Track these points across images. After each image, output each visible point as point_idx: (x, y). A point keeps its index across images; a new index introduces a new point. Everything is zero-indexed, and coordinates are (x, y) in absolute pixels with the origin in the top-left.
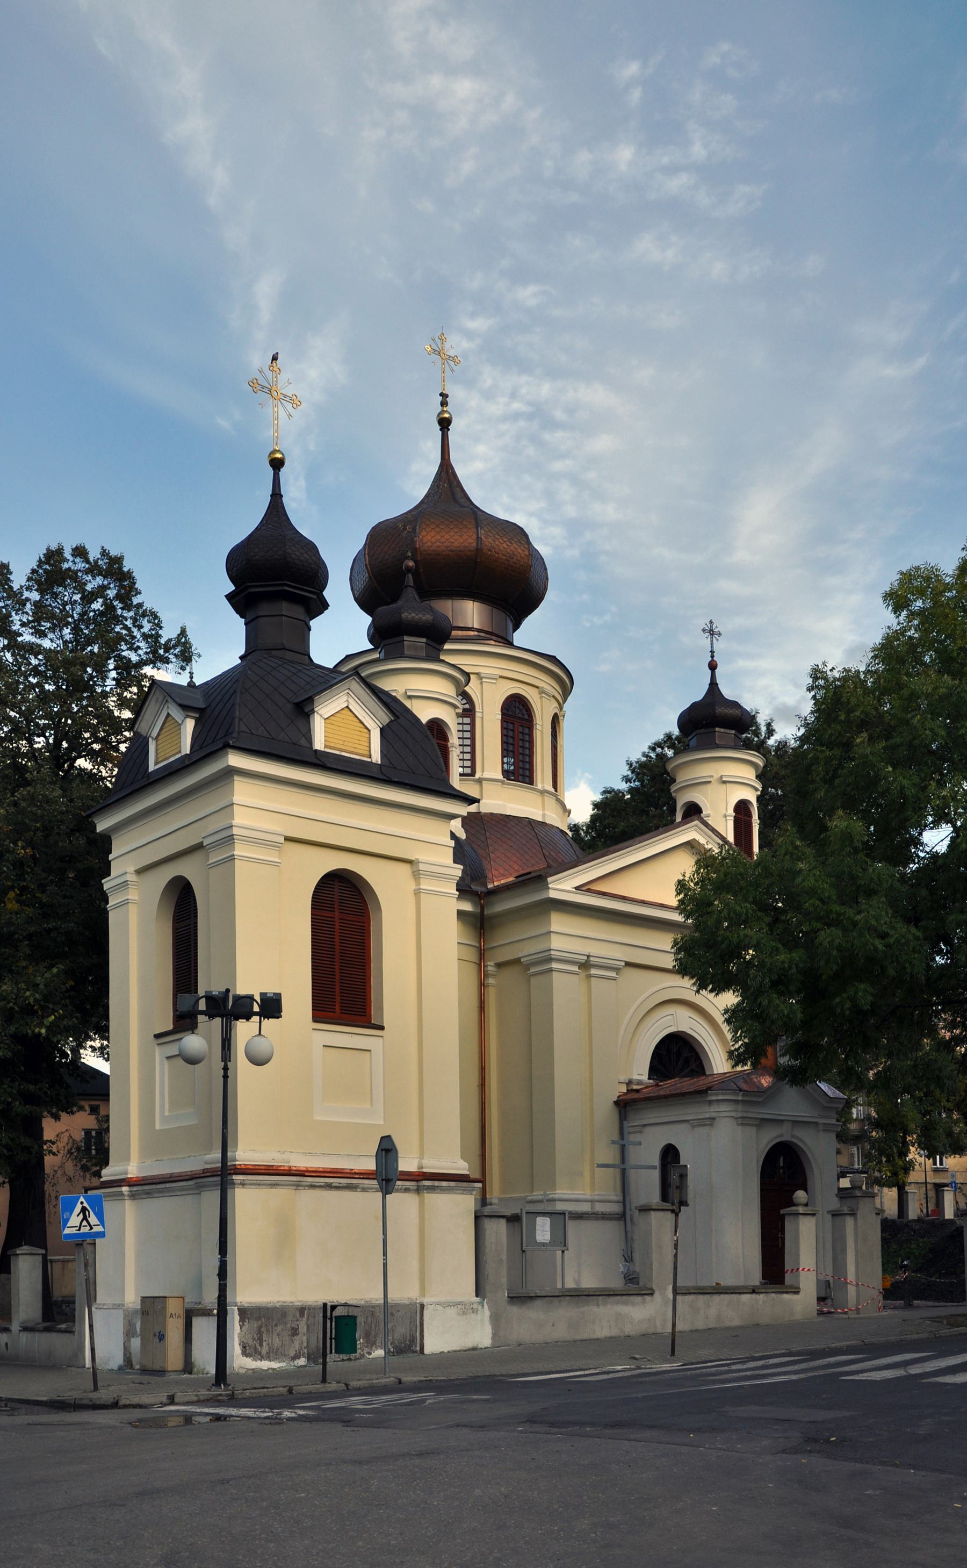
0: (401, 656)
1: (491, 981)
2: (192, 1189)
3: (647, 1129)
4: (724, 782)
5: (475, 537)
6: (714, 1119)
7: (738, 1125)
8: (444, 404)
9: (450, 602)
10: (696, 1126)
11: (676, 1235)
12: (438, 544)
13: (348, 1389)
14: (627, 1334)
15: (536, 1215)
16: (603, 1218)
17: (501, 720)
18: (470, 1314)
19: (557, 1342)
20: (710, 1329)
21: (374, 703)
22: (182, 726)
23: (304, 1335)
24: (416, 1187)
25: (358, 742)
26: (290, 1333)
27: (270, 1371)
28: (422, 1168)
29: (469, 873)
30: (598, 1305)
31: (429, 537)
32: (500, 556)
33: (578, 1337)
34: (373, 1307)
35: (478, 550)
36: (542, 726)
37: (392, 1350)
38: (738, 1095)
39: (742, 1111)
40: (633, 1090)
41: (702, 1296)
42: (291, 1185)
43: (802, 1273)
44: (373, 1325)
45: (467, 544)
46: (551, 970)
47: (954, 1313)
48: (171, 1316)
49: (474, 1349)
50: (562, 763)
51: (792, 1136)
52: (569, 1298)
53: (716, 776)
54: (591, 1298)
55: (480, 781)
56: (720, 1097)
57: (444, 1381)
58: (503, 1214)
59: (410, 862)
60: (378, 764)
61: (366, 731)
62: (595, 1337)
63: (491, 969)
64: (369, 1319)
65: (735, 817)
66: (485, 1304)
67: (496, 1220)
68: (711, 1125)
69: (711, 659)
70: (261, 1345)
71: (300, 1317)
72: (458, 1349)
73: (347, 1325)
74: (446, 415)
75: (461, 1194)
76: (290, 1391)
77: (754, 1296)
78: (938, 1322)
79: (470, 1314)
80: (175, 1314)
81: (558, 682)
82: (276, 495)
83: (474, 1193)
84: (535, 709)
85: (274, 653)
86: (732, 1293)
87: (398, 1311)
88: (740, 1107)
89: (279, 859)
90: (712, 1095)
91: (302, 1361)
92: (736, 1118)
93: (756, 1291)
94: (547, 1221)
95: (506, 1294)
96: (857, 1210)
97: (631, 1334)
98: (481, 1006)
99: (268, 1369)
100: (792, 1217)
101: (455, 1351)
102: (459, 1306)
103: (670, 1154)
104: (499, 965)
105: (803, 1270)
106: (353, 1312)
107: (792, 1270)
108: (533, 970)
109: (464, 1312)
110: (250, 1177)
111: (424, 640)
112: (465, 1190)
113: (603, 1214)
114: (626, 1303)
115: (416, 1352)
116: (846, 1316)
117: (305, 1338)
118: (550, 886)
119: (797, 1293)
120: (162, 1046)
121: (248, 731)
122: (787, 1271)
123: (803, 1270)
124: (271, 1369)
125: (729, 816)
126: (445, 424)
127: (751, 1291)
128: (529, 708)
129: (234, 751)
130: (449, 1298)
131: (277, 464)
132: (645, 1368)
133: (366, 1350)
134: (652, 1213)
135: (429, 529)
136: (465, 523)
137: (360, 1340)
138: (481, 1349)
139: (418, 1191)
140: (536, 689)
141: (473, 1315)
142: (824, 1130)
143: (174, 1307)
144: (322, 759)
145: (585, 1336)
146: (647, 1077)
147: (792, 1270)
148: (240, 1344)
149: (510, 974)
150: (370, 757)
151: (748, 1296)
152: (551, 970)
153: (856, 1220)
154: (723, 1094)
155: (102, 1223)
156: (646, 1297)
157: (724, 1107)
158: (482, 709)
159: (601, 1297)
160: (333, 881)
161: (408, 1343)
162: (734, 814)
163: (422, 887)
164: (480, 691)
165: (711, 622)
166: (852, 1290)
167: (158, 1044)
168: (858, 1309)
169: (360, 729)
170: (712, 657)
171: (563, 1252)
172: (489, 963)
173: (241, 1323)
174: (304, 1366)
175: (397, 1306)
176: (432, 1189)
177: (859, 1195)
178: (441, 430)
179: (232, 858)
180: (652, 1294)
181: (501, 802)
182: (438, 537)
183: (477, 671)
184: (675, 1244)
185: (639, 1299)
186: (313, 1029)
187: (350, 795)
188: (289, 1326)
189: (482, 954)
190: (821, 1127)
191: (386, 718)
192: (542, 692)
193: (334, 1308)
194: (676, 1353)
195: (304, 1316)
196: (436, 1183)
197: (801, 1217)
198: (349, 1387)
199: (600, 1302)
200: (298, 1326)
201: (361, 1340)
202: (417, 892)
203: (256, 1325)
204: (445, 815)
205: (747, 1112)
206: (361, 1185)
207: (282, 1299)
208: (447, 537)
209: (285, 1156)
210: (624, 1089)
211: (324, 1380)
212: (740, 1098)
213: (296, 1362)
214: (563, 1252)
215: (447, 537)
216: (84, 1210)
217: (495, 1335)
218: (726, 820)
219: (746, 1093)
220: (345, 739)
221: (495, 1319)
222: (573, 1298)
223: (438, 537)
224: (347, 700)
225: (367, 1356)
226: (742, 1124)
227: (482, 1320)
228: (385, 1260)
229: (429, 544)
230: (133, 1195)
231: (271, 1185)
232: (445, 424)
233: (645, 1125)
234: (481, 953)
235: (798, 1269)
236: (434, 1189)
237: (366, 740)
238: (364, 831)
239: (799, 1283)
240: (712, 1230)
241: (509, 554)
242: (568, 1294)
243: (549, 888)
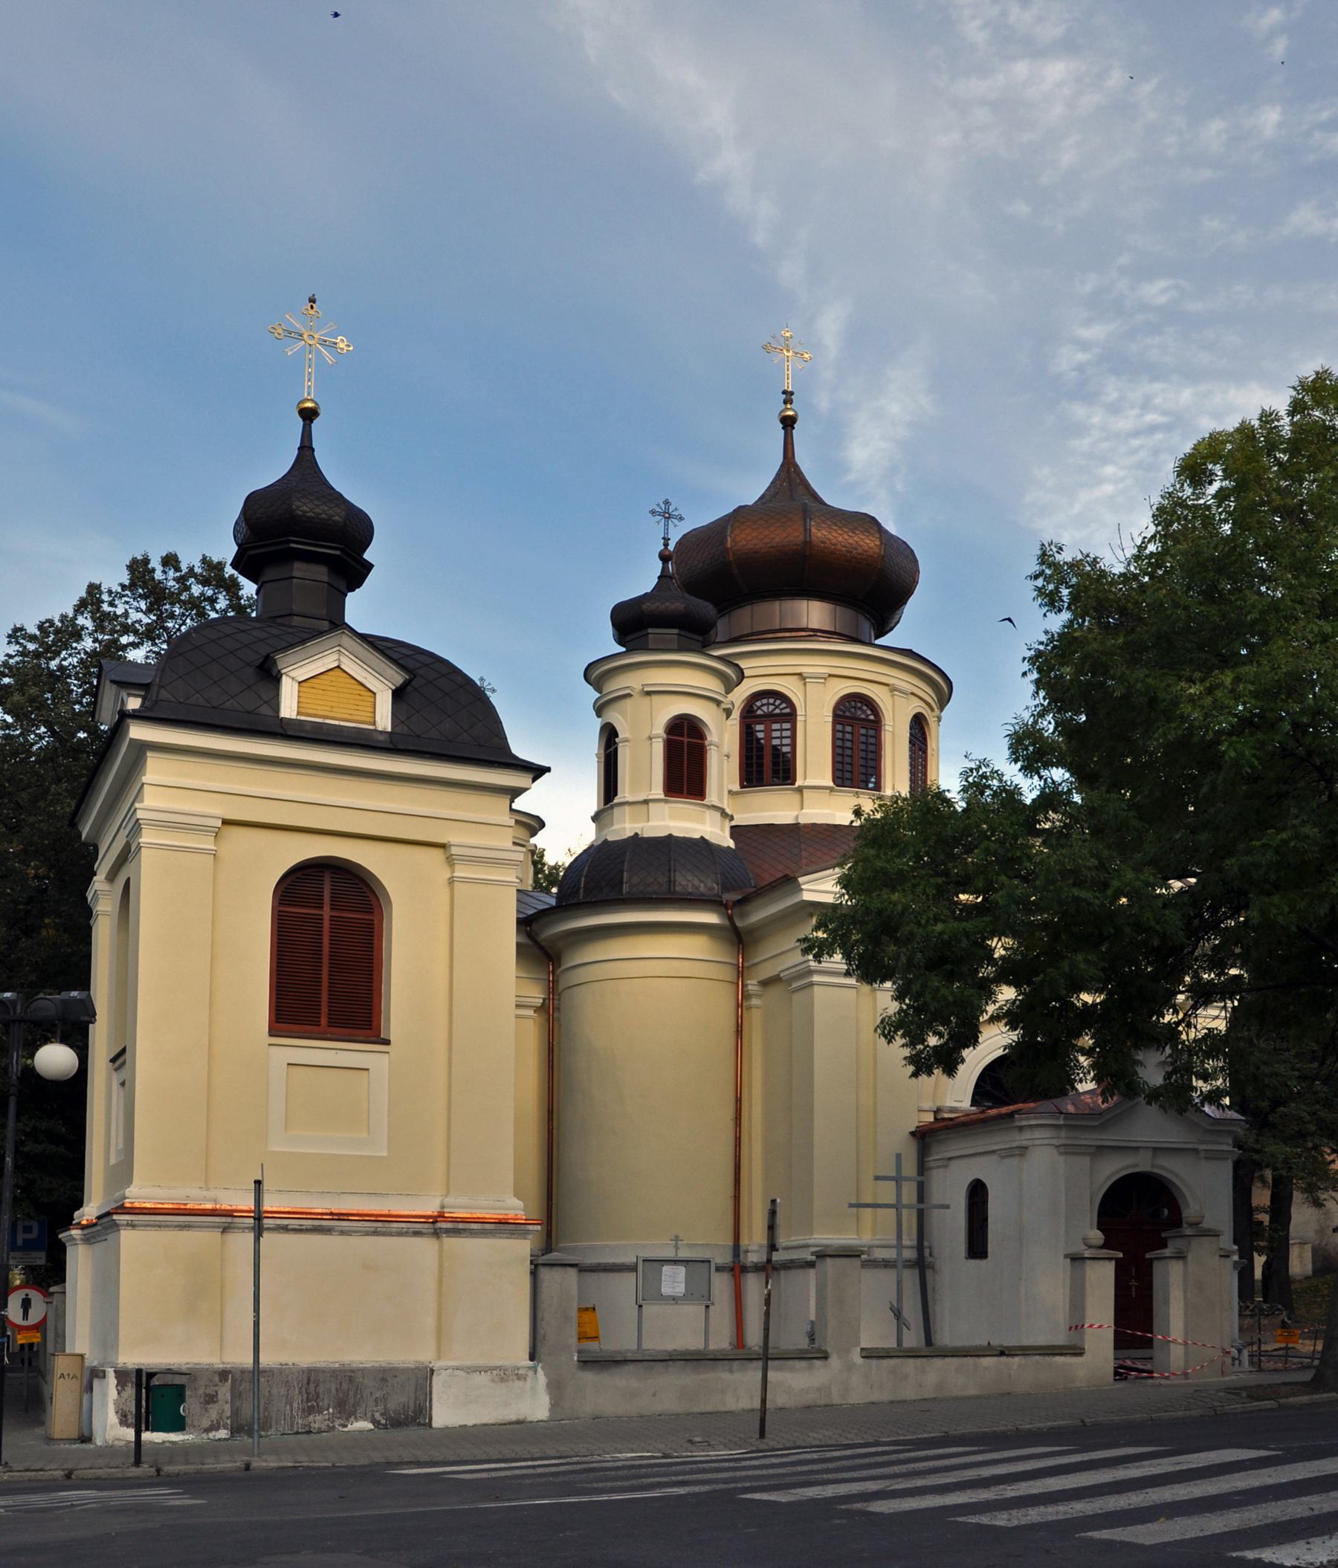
0: (645, 648)
1: (754, 1002)
3: (954, 1164)
4: (649, 693)
5: (801, 529)
6: (1026, 1148)
7: (1061, 1154)
9: (777, 603)
11: (767, 1287)
12: (755, 541)
13: (158, 1475)
14: (780, 1405)
15: (663, 1263)
16: (886, 1266)
17: (796, 715)
18: (513, 1381)
19: (659, 1415)
20: (925, 1400)
21: (378, 661)
23: (227, 1402)
24: (432, 1231)
25: (356, 707)
26: (202, 1400)
27: (167, 1444)
29: (720, 882)
30: (731, 1371)
31: (744, 536)
32: (839, 547)
34: (353, 1371)
35: (807, 543)
36: (893, 727)
37: (383, 1422)
38: (1058, 1118)
39: (1067, 1138)
40: (944, 1119)
41: (911, 1361)
42: (214, 1227)
43: (1088, 1331)
44: (351, 1393)
45: (792, 539)
46: (812, 984)
47: (703, 1411)
48: (62, 1376)
49: (519, 1422)
50: (934, 768)
52: (683, 1362)
53: (638, 687)
55: (800, 790)
57: (326, 1468)
58: (573, 1262)
59: (443, 846)
60: (388, 732)
61: (370, 694)
62: (726, 1409)
63: (752, 985)
64: (345, 1386)
66: (539, 1369)
67: (560, 1270)
68: (1022, 1155)
69: (663, 547)
71: (221, 1381)
72: (492, 1422)
73: (163, 1396)
74: (790, 413)
75: (508, 1238)
76: (247, 1467)
77: (1003, 1359)
78: (1234, 1394)
79: (513, 1381)
80: (69, 1375)
81: (922, 679)
82: (306, 448)
83: (530, 1237)
84: (883, 710)
85: (279, 620)
86: (966, 1356)
87: (396, 1376)
88: (1063, 1134)
89: (215, 846)
90: (1021, 1120)
91: (223, 1434)
93: (1007, 1352)
94: (681, 1270)
95: (576, 1358)
96: (1188, 1252)
97: (788, 1405)
98: (738, 1030)
99: (164, 1442)
101: (485, 1425)
102: (495, 1372)
103: (977, 1193)
104: (765, 983)
106: (178, 1380)
107: (1077, 1327)
108: (795, 985)
109: (502, 1378)
110: (141, 1217)
111: (676, 631)
112: (512, 1234)
113: (883, 1260)
116: (1168, 1382)
117: (227, 1407)
118: (803, 887)
119: (1081, 1354)
121: (174, 700)
123: (1091, 1326)
124: (169, 1442)
126: (788, 423)
127: (998, 1353)
128: (874, 707)
129: (135, 721)
130: (482, 1362)
131: (309, 415)
132: (677, 1457)
134: (829, 1260)
137: (328, 1410)
138: (531, 1422)
140: (886, 687)
141: (518, 1384)
142: (1207, 1158)
146: (970, 1103)
147: (1077, 1327)
148: (117, 1413)
149: (775, 992)
150: (374, 724)
151: (995, 1359)
152: (812, 984)
153: (1186, 1264)
154: (1036, 1118)
156: (815, 1361)
157: (1037, 1134)
158: (806, 712)
160: (323, 872)
161: (410, 1413)
162: (665, 736)
164: (803, 693)
168: (1185, 1375)
169: (359, 692)
171: (707, 1307)
172: (749, 982)
173: (119, 1388)
174: (225, 1439)
175: (269, 1372)
178: (783, 428)
180: (826, 1358)
181: (828, 811)
182: (755, 534)
183: (799, 671)
184: (766, 1300)
185: (803, 1363)
186: (269, 1045)
187: (327, 768)
189: (741, 972)
191: (399, 678)
192: (893, 689)
193: (151, 1375)
195: (227, 1380)
197: (1088, 1262)
198: (162, 1473)
200: (216, 1392)
201: (331, 1410)
202: (451, 881)
204: (500, 789)
206: (336, 1228)
208: (766, 532)
210: (930, 1118)
211: (138, 1462)
212: (1062, 1122)
213: (211, 1435)
214: (707, 1307)
215: (766, 532)
217: (554, 1406)
221: (556, 1388)
222: (688, 1363)
223: (755, 534)
224: (339, 659)
225: (340, 1428)
226: (1066, 1153)
227: (533, 1389)
229: (744, 543)
230: (88, 1240)
231: (179, 1226)
232: (788, 423)
233: (950, 1159)
234: (738, 971)
235: (1083, 1326)
236: (460, 1233)
238: (351, 810)
239: (1084, 1342)
240: (1020, 1279)
241: (851, 544)
242: (679, 1357)
243: (802, 890)
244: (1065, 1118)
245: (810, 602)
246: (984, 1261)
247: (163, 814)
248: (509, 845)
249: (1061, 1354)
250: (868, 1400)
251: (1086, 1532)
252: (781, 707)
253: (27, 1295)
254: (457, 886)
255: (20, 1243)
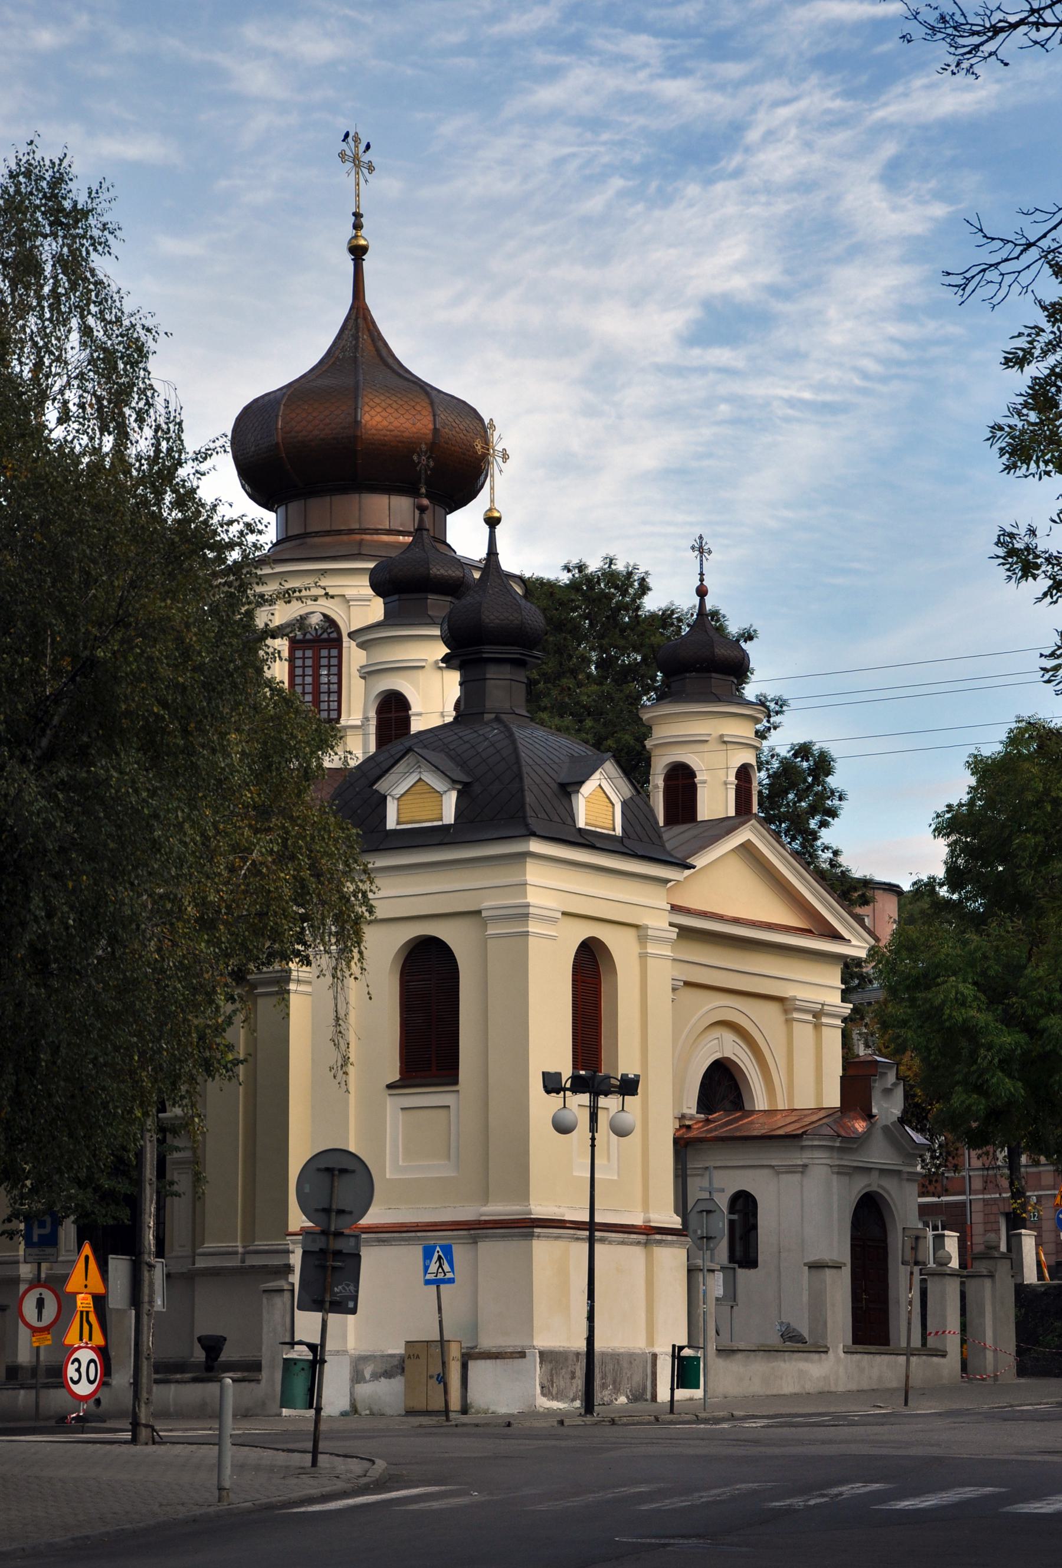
2: (466, 1238)
4: (725, 742)
7: (833, 1173)
8: (357, 226)
10: (783, 1173)
22: (444, 796)
28: (649, 1221)
30: (785, 1361)
33: (769, 1393)
34: (618, 1355)
41: (866, 1356)
51: (879, 1186)
54: (779, 1353)
56: (816, 1143)
59: (636, 926)
61: (610, 805)
62: (783, 1393)
65: (737, 786)
70: (552, 1386)
74: (362, 242)
86: (891, 1354)
88: (835, 1155)
92: (831, 1166)
100: (936, 1278)
105: (949, 1332)
107: (937, 1332)
114: (806, 1360)
115: (646, 1400)
119: (944, 1356)
120: (392, 1097)
122: (930, 1333)
123: (949, 1332)
125: (730, 784)
126: (358, 252)
133: (614, 1396)
135: (373, 413)
136: (418, 408)
139: (646, 1244)
142: (908, 1180)
143: (455, 1351)
144: (589, 838)
145: (775, 1392)
147: (937, 1332)
153: (994, 1282)
154: (820, 1140)
155: (453, 1271)
157: (817, 1154)
159: (787, 1354)
162: (736, 782)
163: (649, 951)
165: (701, 537)
166: (989, 1355)
167: (390, 1095)
170: (702, 580)
171: (732, 1307)
176: (659, 1242)
177: (997, 1256)
179: (526, 934)
180: (826, 1352)
185: (815, 1356)
188: (569, 1369)
190: (905, 1176)
194: (910, 1404)
196: (664, 1237)
199: (786, 1358)
203: (549, 1367)
205: (842, 1159)
207: (562, 1344)
209: (561, 1210)
212: (838, 1144)
214: (732, 1307)
216: (440, 1258)
218: (727, 788)
219: (844, 1139)
220: (597, 815)
226: (838, 1173)
228: (441, 1317)
232: (358, 252)
235: (944, 1332)
237: (611, 813)
244: (841, 1142)
245: (334, 498)
246: (752, 1271)
247: (546, 911)
248: (666, 926)
249: (936, 1355)
250: (848, 1389)
251: (1000, 1493)
252: (329, 631)
253: (41, 1294)
254: (650, 961)
255: (35, 1239)
